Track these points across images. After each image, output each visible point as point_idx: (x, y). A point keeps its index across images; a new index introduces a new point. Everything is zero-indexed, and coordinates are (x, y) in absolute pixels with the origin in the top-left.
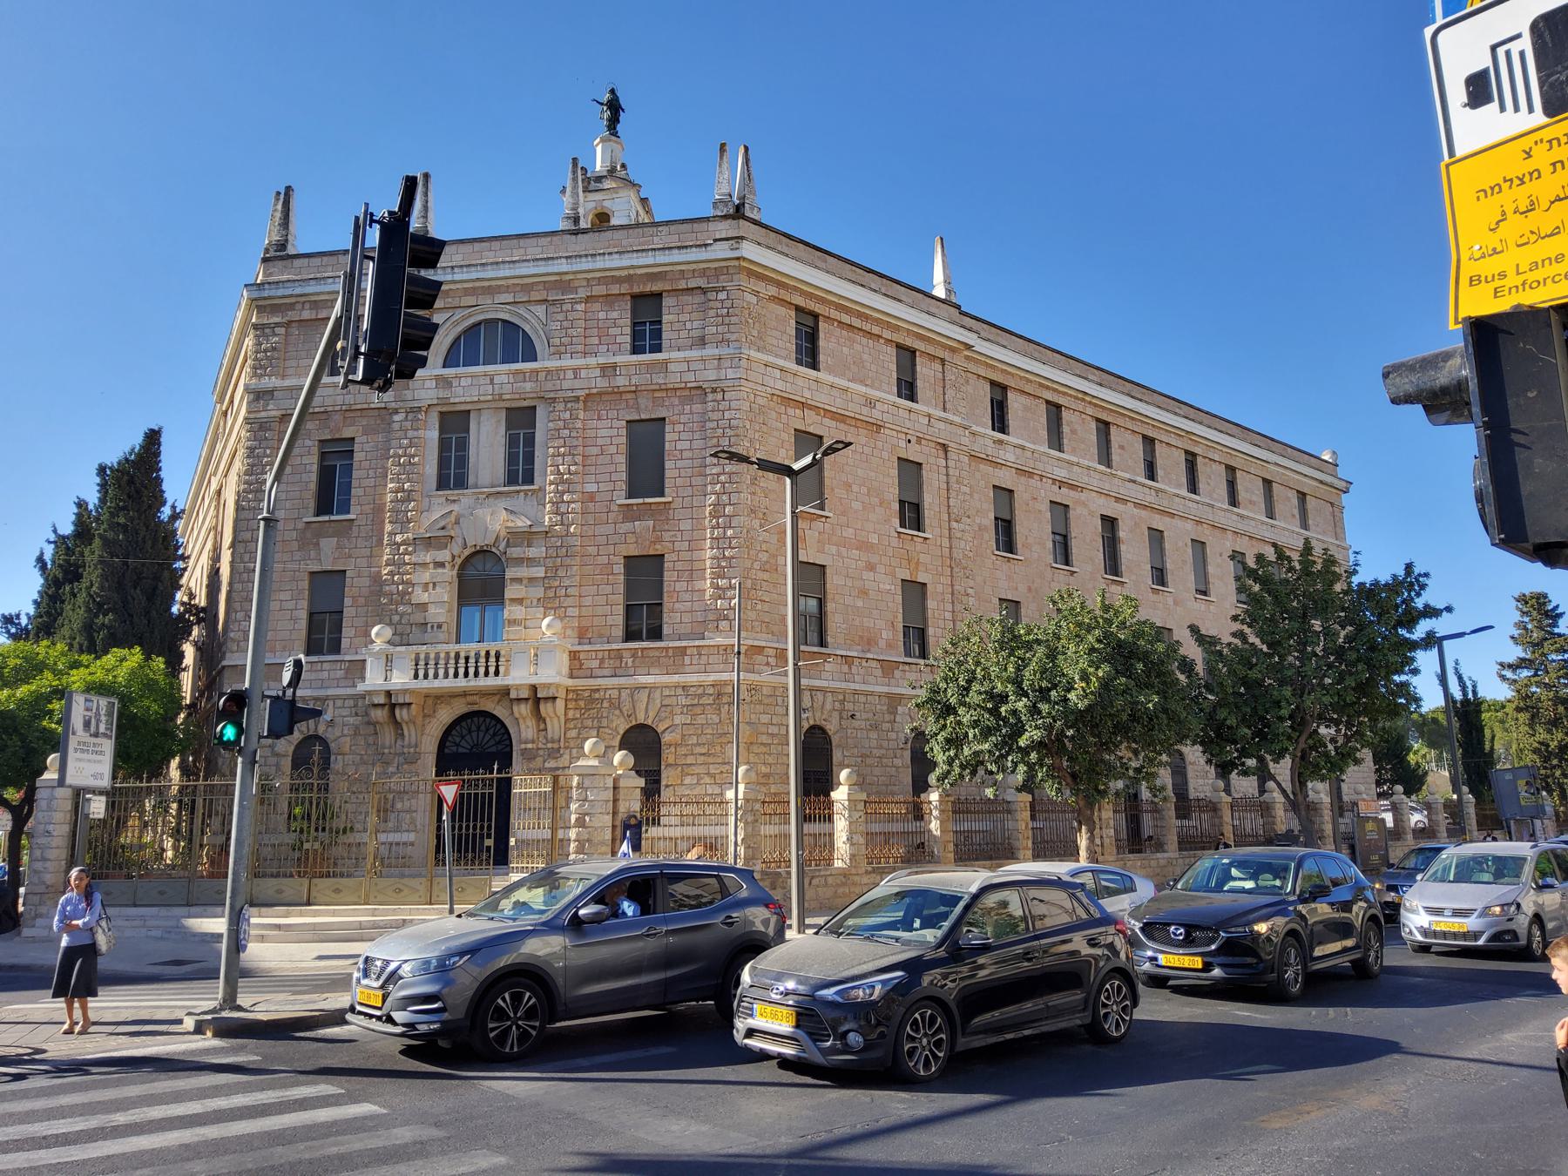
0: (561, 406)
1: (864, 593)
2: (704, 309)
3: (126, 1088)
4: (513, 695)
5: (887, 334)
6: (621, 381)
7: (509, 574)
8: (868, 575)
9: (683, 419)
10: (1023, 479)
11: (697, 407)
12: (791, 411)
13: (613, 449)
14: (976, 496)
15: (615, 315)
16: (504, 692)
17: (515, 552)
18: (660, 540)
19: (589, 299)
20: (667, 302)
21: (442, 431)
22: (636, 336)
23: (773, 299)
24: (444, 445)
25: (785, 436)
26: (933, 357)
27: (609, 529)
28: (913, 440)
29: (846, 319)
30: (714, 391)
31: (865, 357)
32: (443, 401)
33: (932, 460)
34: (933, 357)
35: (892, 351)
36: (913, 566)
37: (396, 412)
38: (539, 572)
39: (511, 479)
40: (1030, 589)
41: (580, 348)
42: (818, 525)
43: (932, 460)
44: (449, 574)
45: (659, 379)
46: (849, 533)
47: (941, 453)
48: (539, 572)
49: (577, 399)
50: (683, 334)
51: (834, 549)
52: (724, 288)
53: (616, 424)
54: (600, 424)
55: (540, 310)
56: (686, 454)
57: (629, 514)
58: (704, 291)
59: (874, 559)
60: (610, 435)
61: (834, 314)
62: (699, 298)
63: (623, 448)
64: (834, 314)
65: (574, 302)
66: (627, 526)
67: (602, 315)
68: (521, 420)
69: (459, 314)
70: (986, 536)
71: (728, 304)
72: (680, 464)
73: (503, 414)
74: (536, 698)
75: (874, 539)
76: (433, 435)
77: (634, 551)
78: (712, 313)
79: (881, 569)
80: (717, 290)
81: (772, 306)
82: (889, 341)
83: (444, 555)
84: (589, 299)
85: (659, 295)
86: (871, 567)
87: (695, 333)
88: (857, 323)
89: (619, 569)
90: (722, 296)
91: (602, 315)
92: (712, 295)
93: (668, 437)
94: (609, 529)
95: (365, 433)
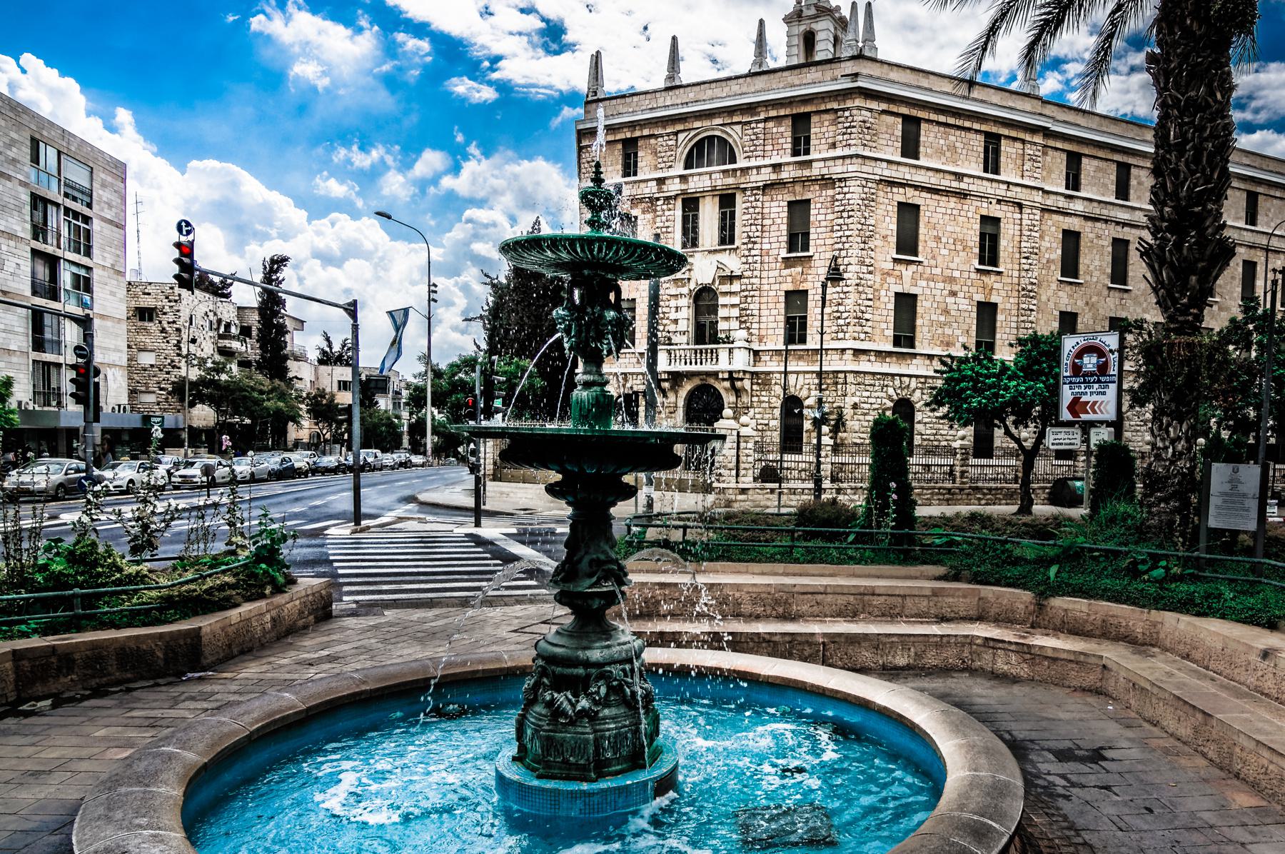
0: (748, 193)
1: (946, 312)
2: (835, 122)
3: (87, 634)
4: (720, 376)
5: (976, 126)
6: (784, 175)
7: (722, 300)
8: (950, 300)
9: (821, 200)
10: (1090, 224)
11: (830, 192)
12: (895, 190)
13: (779, 221)
14: (1047, 238)
15: (782, 129)
16: (715, 374)
17: (725, 288)
18: (806, 280)
19: (766, 120)
20: (814, 119)
21: (684, 211)
22: (796, 142)
23: (884, 112)
24: (685, 219)
25: (890, 208)
26: (1015, 139)
27: (776, 273)
28: (994, 201)
29: (942, 119)
30: (840, 180)
31: (958, 144)
32: (684, 192)
33: (1009, 215)
34: (1015, 139)
35: (981, 138)
36: (987, 291)
37: (658, 199)
38: (736, 300)
39: (722, 241)
40: (1087, 303)
41: (761, 153)
42: (913, 268)
43: (1009, 215)
44: (684, 302)
45: (806, 173)
46: (938, 271)
47: (1017, 210)
48: (736, 300)
49: (758, 188)
50: (823, 141)
51: (924, 283)
52: (848, 109)
53: (783, 204)
54: (773, 204)
55: (738, 128)
56: (823, 224)
57: (788, 263)
58: (836, 111)
59: (955, 288)
60: (777, 209)
61: (933, 117)
62: (831, 117)
63: (785, 220)
64: (933, 117)
65: (758, 122)
66: (785, 272)
67: (775, 130)
68: (727, 201)
69: (693, 133)
70: (1053, 267)
71: (850, 119)
72: (819, 230)
73: (717, 199)
74: (732, 377)
75: (957, 274)
76: (679, 213)
77: (790, 287)
78: (840, 126)
79: (961, 295)
80: (843, 110)
81: (884, 117)
82: (977, 131)
83: (685, 290)
84: (766, 120)
85: (807, 116)
86: (953, 294)
87: (830, 141)
88: (951, 121)
89: (782, 299)
90: (847, 114)
91: (775, 130)
92: (840, 113)
93: (812, 212)
94: (776, 273)
95: (643, 212)
